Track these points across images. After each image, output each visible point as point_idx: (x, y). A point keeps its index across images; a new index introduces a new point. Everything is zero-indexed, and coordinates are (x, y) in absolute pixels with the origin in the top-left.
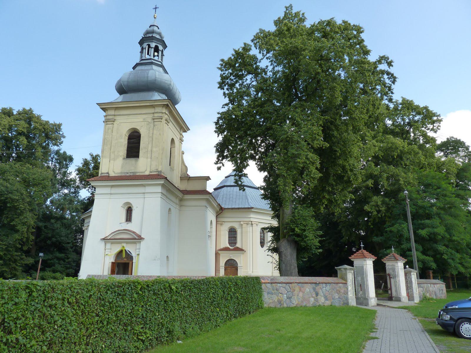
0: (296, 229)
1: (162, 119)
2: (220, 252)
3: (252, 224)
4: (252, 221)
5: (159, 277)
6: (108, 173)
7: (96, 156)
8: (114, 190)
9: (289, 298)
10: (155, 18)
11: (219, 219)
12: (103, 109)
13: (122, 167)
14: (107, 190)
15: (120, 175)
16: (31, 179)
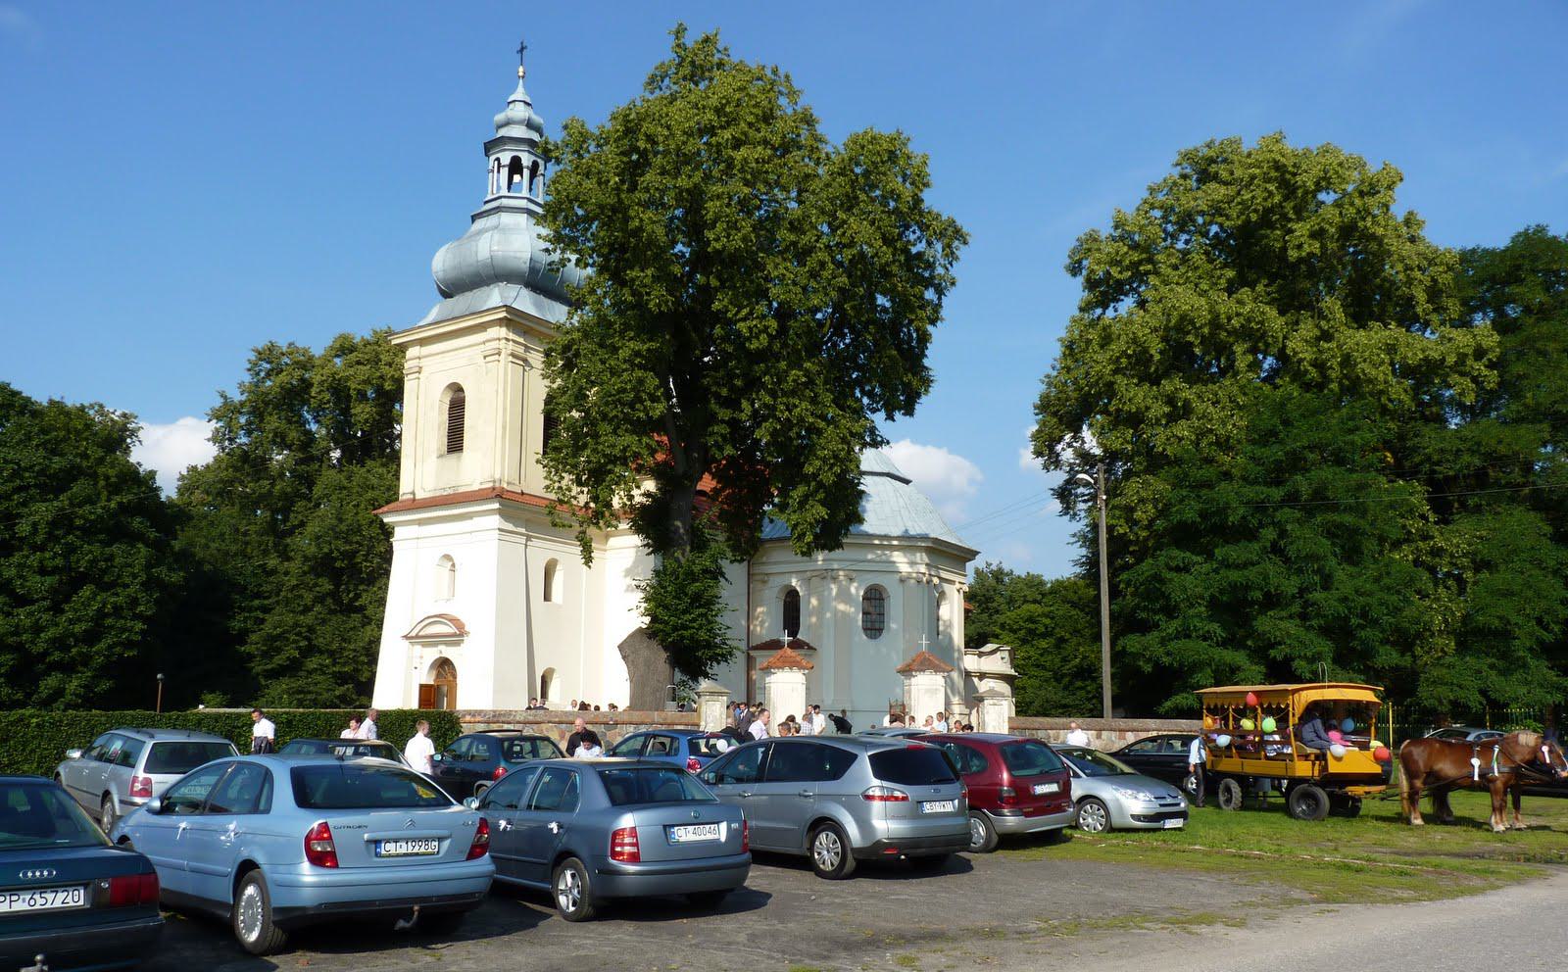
1: (499, 354)
2: (752, 653)
5: (497, 717)
11: (757, 570)
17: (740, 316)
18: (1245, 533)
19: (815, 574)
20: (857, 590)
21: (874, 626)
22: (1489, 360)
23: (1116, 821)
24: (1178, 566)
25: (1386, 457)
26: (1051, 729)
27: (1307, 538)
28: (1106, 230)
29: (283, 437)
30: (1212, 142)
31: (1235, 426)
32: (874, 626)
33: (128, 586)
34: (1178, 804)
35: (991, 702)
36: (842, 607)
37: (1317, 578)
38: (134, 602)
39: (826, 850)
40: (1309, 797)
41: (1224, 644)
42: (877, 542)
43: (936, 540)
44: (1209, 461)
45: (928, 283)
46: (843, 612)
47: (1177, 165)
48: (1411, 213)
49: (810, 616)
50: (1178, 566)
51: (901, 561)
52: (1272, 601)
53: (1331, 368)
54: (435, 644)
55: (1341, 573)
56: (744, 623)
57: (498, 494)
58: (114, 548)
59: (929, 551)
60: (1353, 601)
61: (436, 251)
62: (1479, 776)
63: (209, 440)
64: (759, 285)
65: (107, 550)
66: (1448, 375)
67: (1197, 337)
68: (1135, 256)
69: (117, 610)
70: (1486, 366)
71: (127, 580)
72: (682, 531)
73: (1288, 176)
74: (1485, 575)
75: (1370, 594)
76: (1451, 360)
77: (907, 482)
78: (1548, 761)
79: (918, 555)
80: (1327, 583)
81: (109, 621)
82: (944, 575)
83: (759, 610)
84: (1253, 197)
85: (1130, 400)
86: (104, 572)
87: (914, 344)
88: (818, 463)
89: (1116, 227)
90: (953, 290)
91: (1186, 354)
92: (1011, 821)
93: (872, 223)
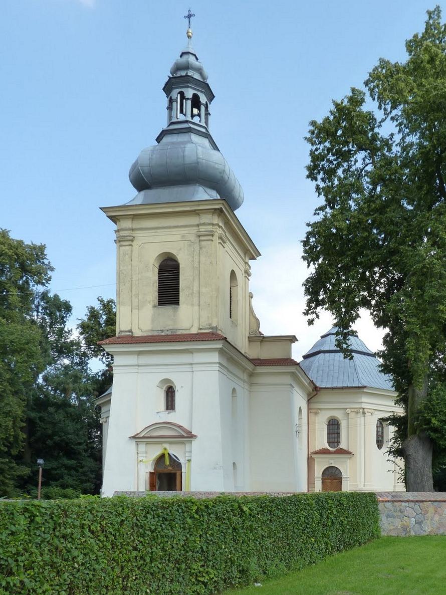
0: (434, 420)
3: (364, 413)
4: (363, 409)
6: (130, 331)
7: (109, 302)
8: (144, 360)
9: (419, 523)
10: (189, 37)
12: (111, 218)
13: (153, 321)
14: (132, 360)
15: (150, 334)
16: (7, 342)
54: (161, 443)
57: (211, 336)
87: (412, 269)
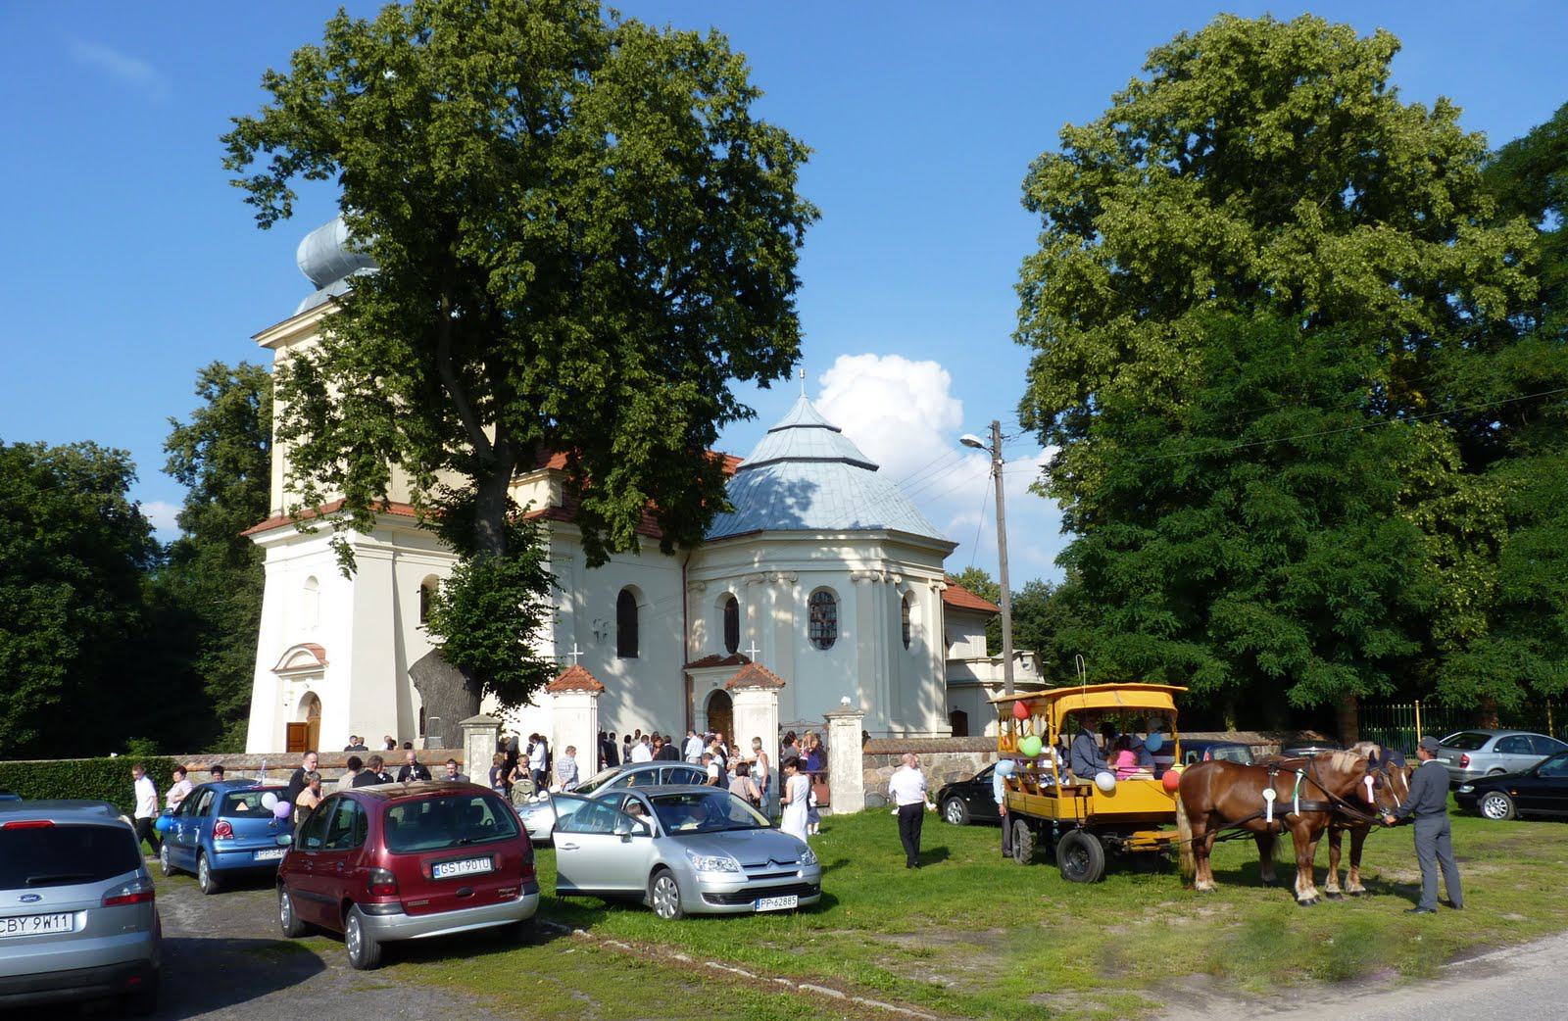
2: (690, 672)
17: (494, 261)
18: (1197, 497)
19: (754, 577)
20: (801, 596)
21: (825, 633)
22: (1526, 264)
23: (689, 906)
24: (1122, 543)
25: (1415, 397)
26: (921, 752)
27: (1270, 496)
28: (1055, 148)
29: (235, 461)
30: (1184, 35)
31: (1188, 366)
32: (825, 633)
33: (45, 628)
34: (794, 874)
35: (840, 722)
36: (783, 616)
37: (1283, 548)
38: (53, 645)
39: (663, 902)
40: (1078, 847)
41: (1179, 636)
42: (820, 537)
43: (891, 532)
44: (1156, 411)
45: (786, 218)
46: (784, 622)
47: (1148, 68)
48: (1441, 100)
49: (749, 627)
50: (1122, 543)
51: (852, 558)
52: (1225, 579)
53: (1307, 286)
54: (303, 677)
55: (1319, 542)
56: (679, 637)
58: (32, 589)
59: (884, 544)
60: (1327, 573)
61: (297, 244)
62: (1275, 815)
63: (164, 471)
64: (511, 222)
65: (23, 592)
66: (1471, 287)
67: (1143, 262)
68: (1089, 178)
69: (34, 655)
70: (1521, 273)
71: (45, 622)
72: (489, 532)
73: (1253, 58)
74: (1522, 532)
75: (1351, 565)
76: (1472, 266)
77: (874, 468)
78: (1371, 800)
79: (872, 550)
80: (1298, 550)
81: (25, 667)
82: (908, 571)
83: (698, 623)
84: (1209, 86)
85: (1070, 346)
86: (18, 614)
88: (624, 439)
89: (1066, 145)
90: (817, 224)
91: (1156, 285)
92: (392, 921)
93: (651, 135)
